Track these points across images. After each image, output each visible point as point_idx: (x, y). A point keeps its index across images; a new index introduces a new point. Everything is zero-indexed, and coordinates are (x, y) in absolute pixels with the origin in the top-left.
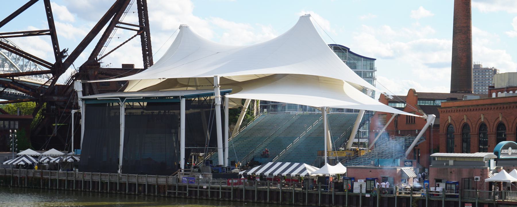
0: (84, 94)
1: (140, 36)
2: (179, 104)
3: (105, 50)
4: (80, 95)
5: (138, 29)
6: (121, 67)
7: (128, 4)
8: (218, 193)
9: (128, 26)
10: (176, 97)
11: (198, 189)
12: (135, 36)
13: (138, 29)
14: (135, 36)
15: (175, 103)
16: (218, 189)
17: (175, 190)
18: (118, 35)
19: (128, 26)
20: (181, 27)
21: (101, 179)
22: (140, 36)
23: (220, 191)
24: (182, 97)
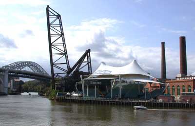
3: (80, 67)
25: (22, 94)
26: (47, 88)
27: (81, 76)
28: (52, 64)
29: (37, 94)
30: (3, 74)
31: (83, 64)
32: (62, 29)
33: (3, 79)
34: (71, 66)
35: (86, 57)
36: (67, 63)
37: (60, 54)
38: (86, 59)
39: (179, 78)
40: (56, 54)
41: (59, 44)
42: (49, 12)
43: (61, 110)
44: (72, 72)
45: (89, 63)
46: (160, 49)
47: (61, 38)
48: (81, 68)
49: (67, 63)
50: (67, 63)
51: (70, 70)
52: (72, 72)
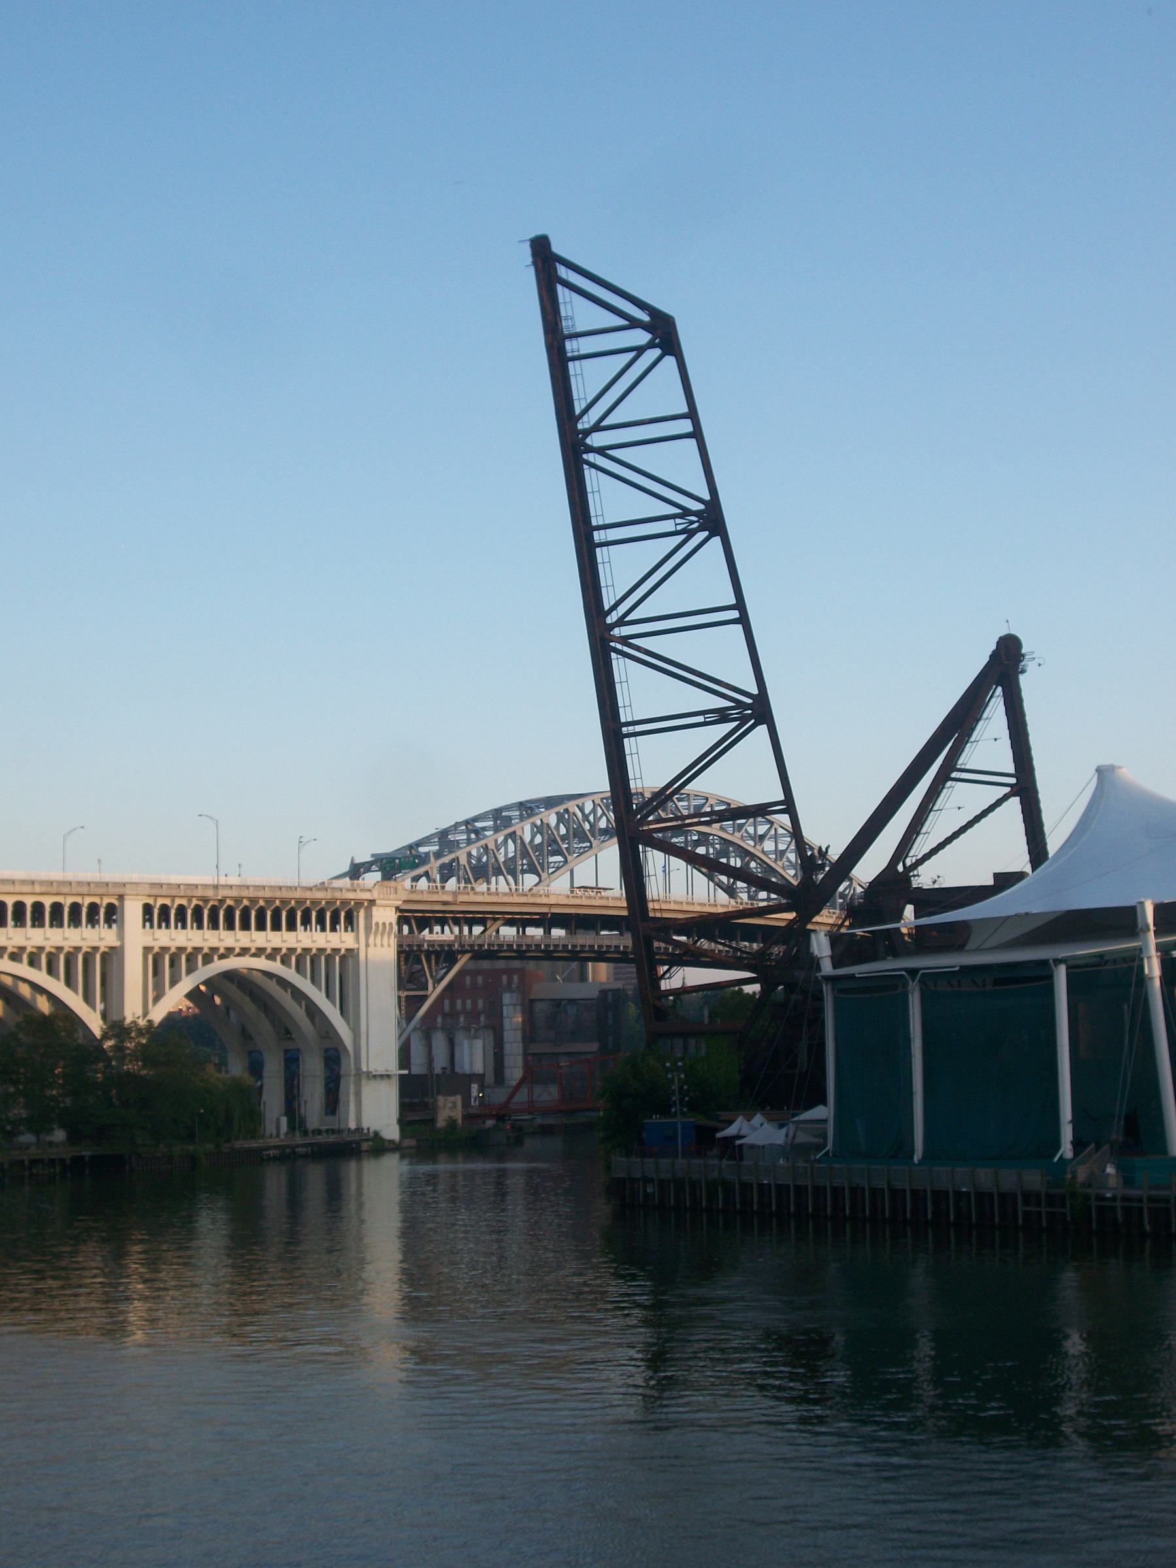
0: (837, 962)
1: (1017, 799)
2: (1049, 978)
3: (921, 846)
4: (827, 968)
5: (1013, 781)
6: (991, 882)
7: (979, 719)
8: (1141, 1209)
9: (983, 778)
10: (1044, 963)
11: (1118, 1203)
12: (999, 803)
13: (1013, 781)
14: (999, 803)
15: (1041, 973)
16: (1140, 1200)
17: (1039, 1205)
18: (960, 801)
19: (983, 778)
20: (1099, 771)
21: (888, 1183)
22: (1017, 799)
23: (1145, 1205)
24: (1058, 961)
30: (341, 939)
38: (989, 746)
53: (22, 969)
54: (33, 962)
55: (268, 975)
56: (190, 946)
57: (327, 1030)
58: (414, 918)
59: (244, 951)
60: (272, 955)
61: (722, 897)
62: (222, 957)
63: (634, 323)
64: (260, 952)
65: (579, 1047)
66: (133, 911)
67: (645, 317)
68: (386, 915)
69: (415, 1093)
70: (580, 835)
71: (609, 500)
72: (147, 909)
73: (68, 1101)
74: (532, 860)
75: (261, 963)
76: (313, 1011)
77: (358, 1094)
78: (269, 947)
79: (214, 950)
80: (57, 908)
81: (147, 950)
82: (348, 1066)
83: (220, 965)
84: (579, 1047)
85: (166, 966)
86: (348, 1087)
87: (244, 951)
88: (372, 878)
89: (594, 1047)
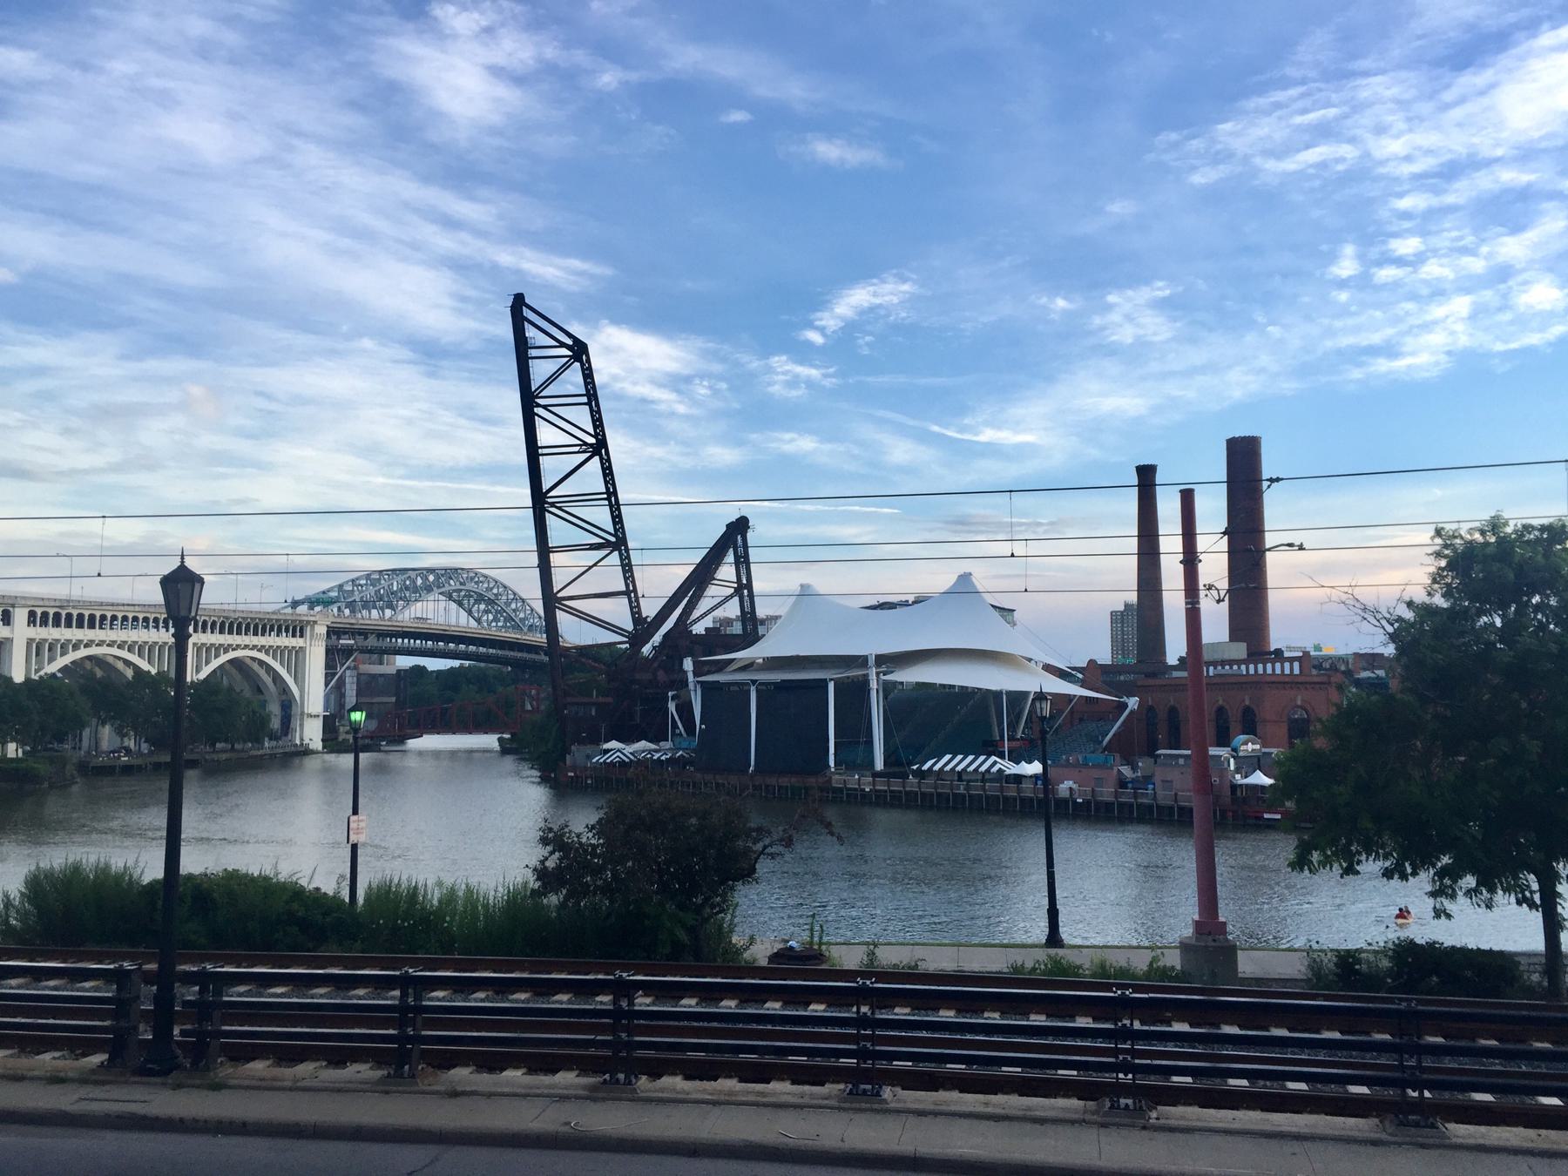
3: (696, 614)
25: (413, 744)
26: (781, 849)
27: (688, 664)
28: (551, 600)
29: (490, 741)
30: (297, 642)
31: (714, 592)
32: (598, 422)
33: (299, 677)
34: (650, 610)
35: (730, 557)
36: (627, 593)
37: (593, 547)
38: (727, 571)
39: (1239, 662)
40: (557, 450)
41: (585, 498)
42: (530, 332)
43: (450, 268)
44: (657, 638)
45: (744, 589)
46: (1129, 504)
47: (596, 459)
48: (695, 622)
49: (627, 593)
50: (630, 592)
51: (643, 628)
52: (657, 638)
53: (115, 651)
54: (267, 653)
55: (253, 659)
56: (151, 641)
57: (284, 690)
58: (333, 632)
59: (246, 647)
60: (266, 650)
61: (473, 623)
62: (86, 646)
63: (562, 345)
64: (254, 647)
65: (385, 699)
66: (20, 616)
67: (570, 342)
68: (321, 630)
69: (330, 727)
70: (416, 590)
71: (547, 435)
72: (32, 614)
73: (1374, 698)
74: (388, 600)
75: (115, 651)
76: (277, 678)
77: (302, 726)
78: (108, 640)
79: (80, 641)
80: (146, 620)
81: (30, 642)
82: (295, 710)
83: (231, 655)
84: (385, 699)
85: (37, 649)
86: (295, 723)
87: (246, 647)
88: (303, 609)
89: (393, 699)
